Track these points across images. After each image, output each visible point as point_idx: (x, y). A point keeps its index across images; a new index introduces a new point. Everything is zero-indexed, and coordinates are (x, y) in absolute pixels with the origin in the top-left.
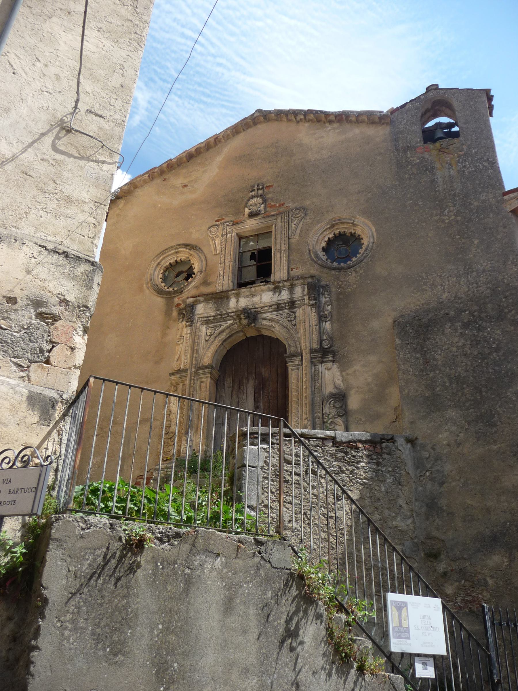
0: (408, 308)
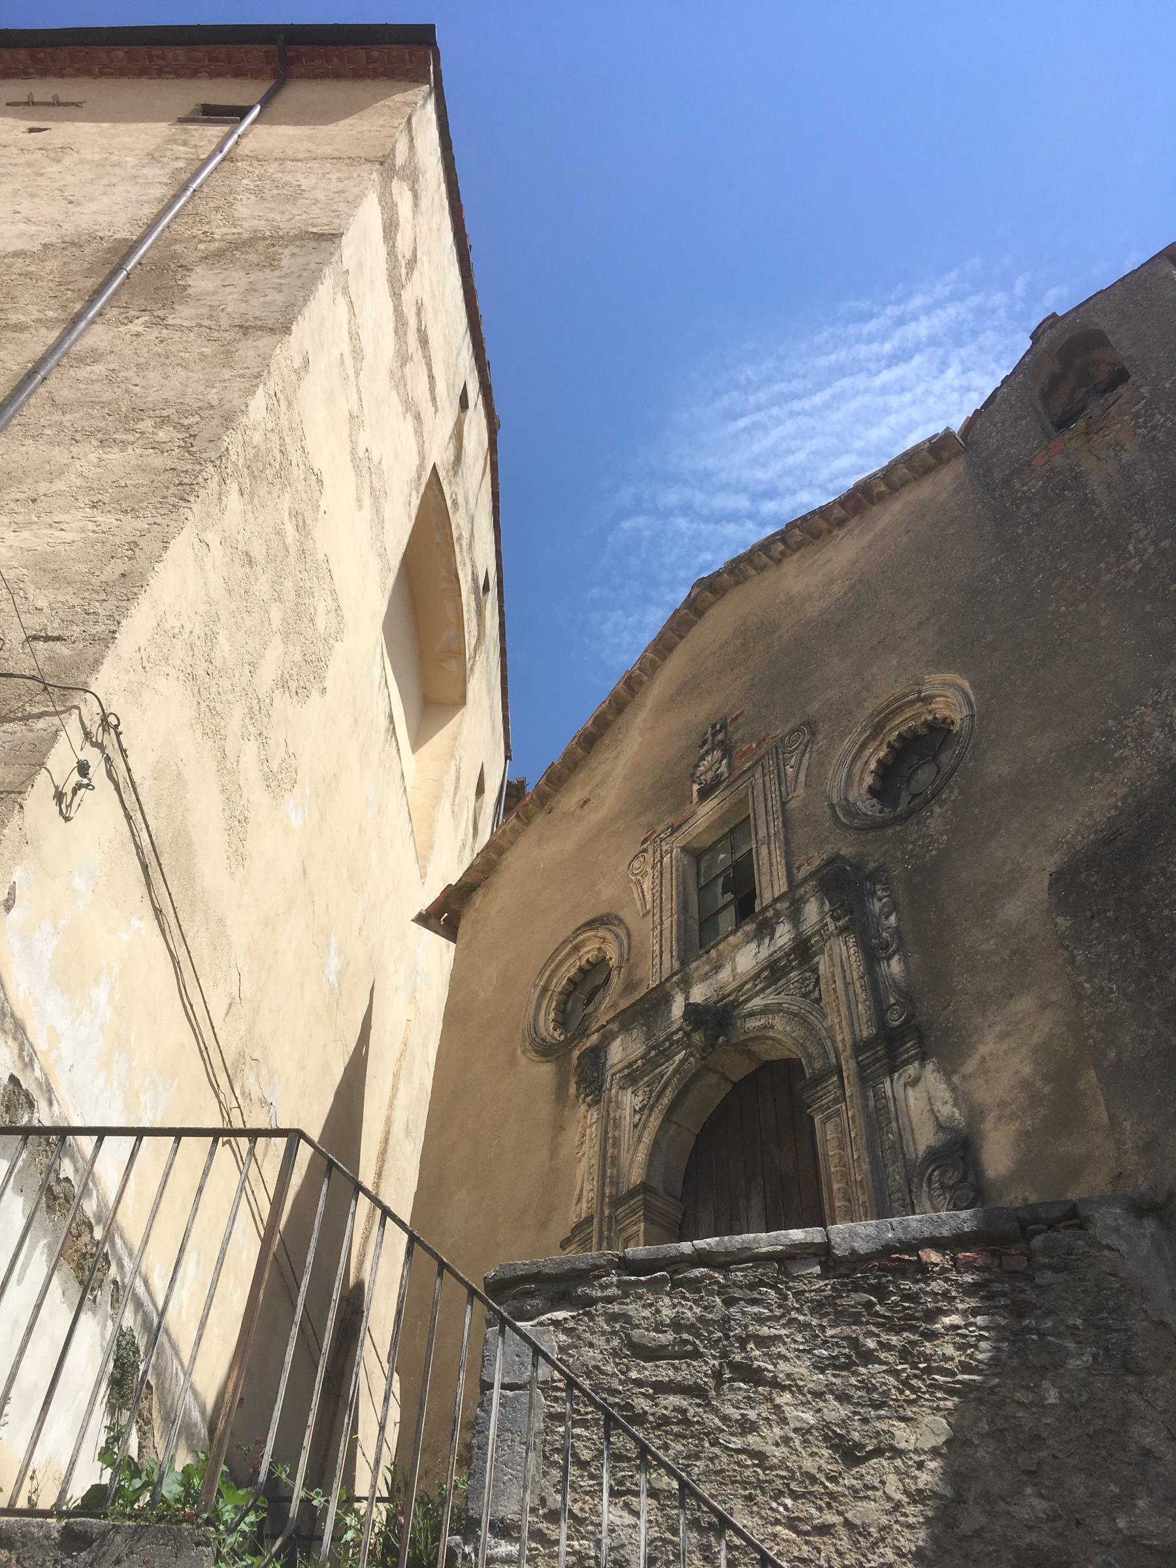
0: (1087, 827)
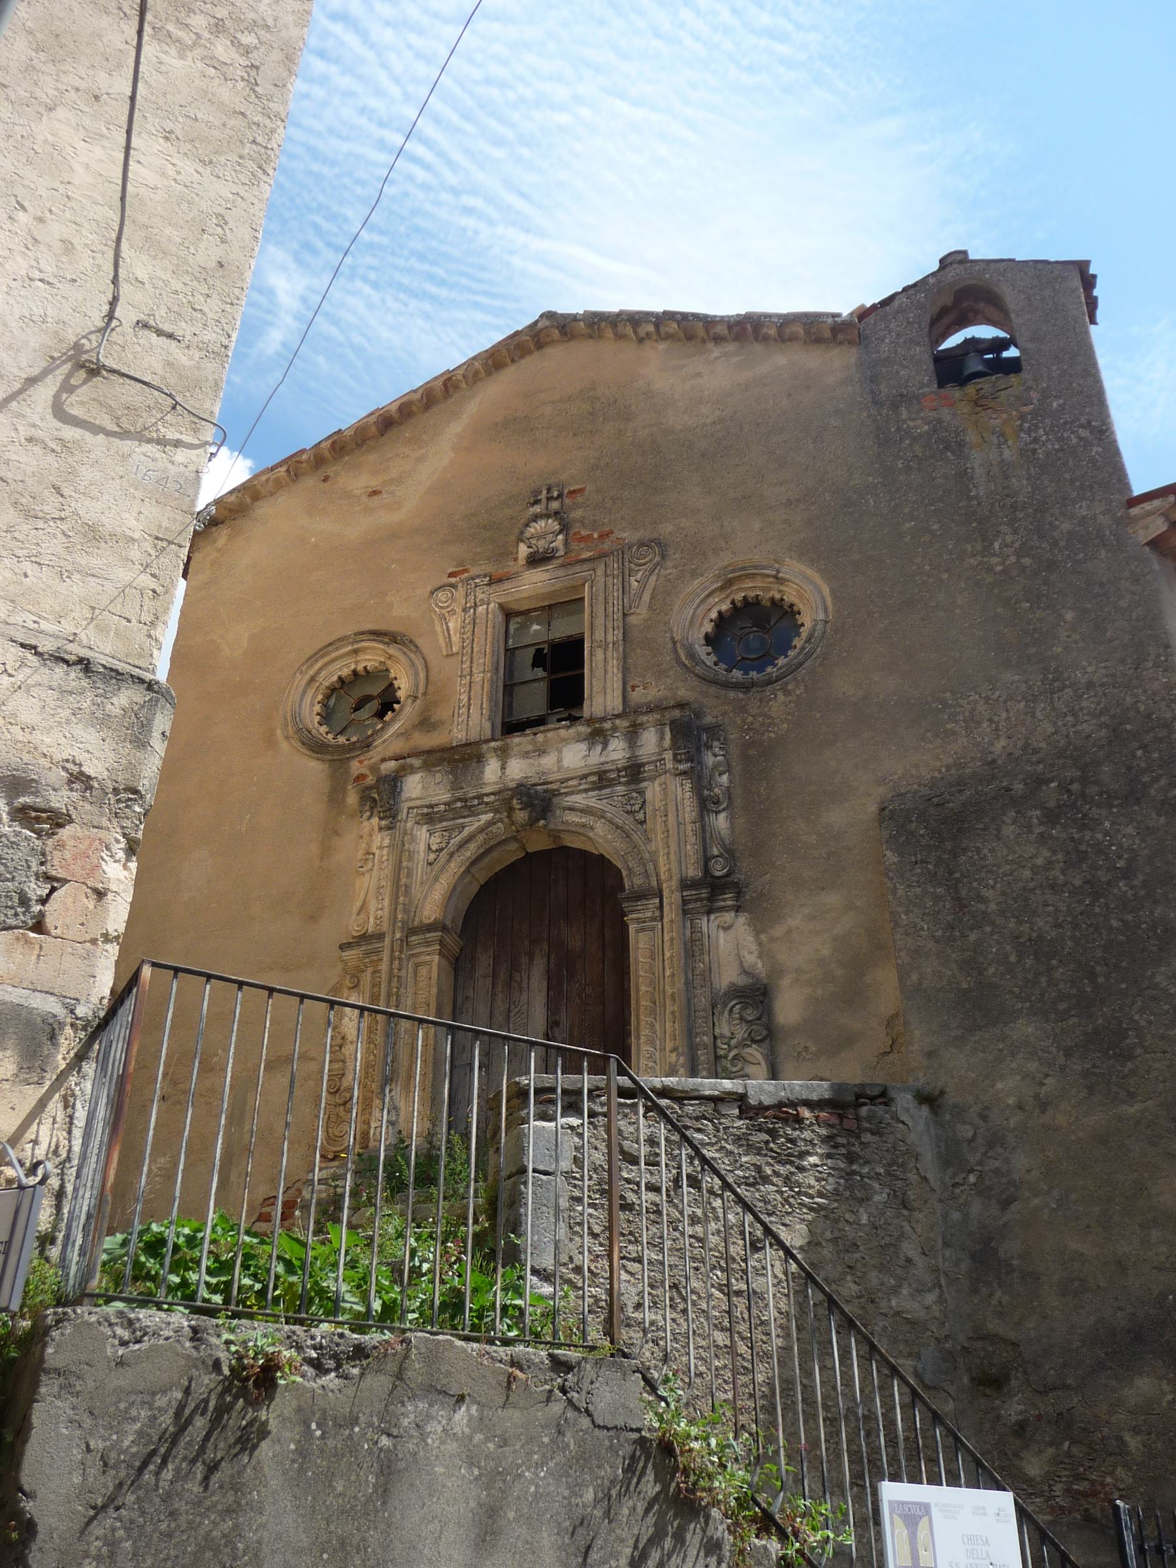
0: (912, 776)
